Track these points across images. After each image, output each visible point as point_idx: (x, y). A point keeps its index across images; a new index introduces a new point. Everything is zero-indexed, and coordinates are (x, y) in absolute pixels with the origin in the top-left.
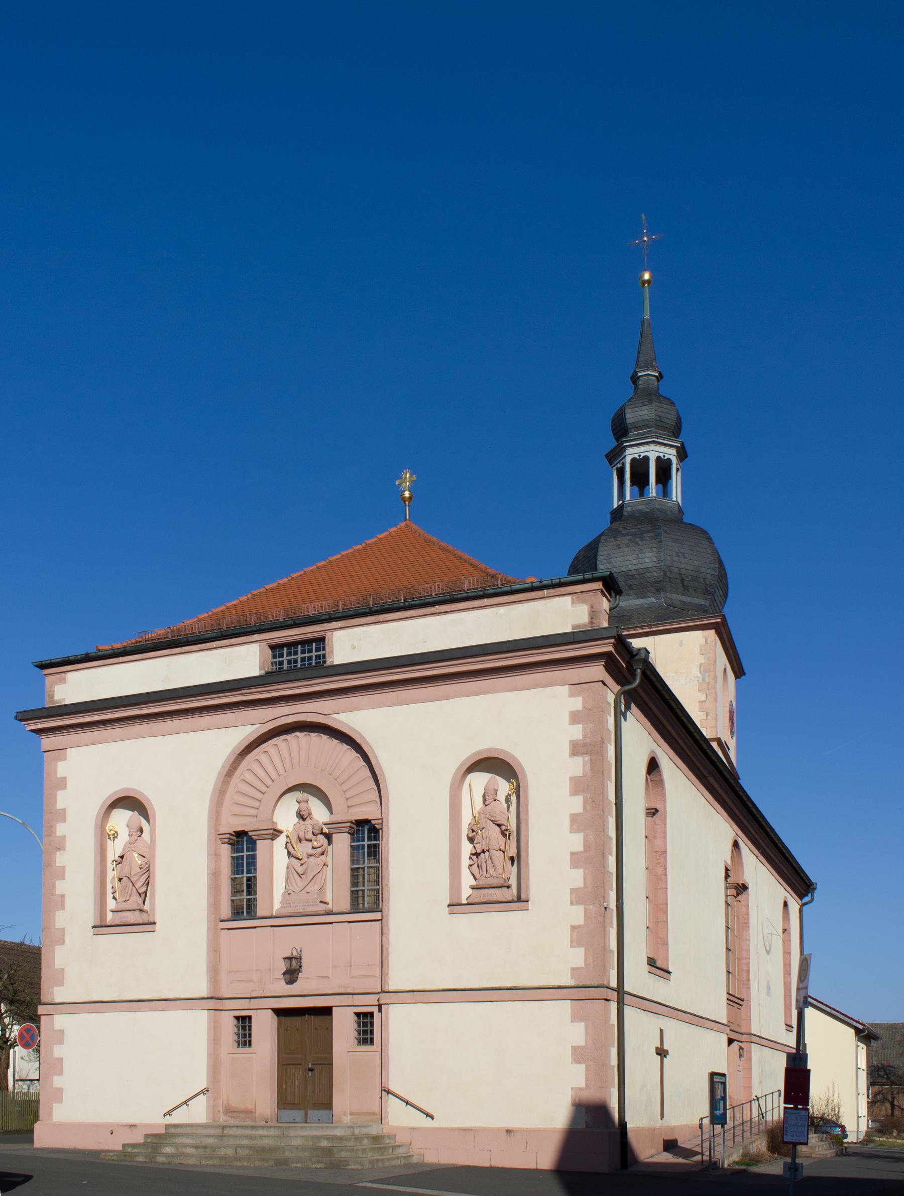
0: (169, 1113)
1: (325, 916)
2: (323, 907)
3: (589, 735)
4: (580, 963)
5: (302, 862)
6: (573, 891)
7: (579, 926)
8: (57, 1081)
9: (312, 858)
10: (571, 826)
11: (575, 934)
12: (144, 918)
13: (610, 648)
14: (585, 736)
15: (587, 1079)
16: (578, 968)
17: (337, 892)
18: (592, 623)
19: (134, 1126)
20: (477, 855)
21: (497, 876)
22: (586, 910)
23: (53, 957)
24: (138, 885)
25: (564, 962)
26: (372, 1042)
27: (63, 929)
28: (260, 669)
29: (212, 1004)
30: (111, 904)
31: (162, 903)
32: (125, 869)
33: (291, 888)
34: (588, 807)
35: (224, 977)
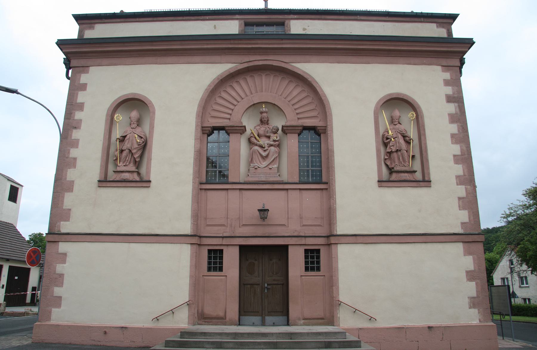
0: (157, 319)
4: (466, 220)
6: (457, 177)
7: (463, 198)
9: (272, 148)
10: (452, 140)
11: (461, 202)
14: (454, 94)
15: (477, 291)
16: (465, 223)
19: (126, 328)
20: (390, 153)
22: (466, 189)
23: (63, 202)
26: (318, 269)
27: (73, 181)
29: (195, 240)
30: (111, 168)
34: (461, 131)
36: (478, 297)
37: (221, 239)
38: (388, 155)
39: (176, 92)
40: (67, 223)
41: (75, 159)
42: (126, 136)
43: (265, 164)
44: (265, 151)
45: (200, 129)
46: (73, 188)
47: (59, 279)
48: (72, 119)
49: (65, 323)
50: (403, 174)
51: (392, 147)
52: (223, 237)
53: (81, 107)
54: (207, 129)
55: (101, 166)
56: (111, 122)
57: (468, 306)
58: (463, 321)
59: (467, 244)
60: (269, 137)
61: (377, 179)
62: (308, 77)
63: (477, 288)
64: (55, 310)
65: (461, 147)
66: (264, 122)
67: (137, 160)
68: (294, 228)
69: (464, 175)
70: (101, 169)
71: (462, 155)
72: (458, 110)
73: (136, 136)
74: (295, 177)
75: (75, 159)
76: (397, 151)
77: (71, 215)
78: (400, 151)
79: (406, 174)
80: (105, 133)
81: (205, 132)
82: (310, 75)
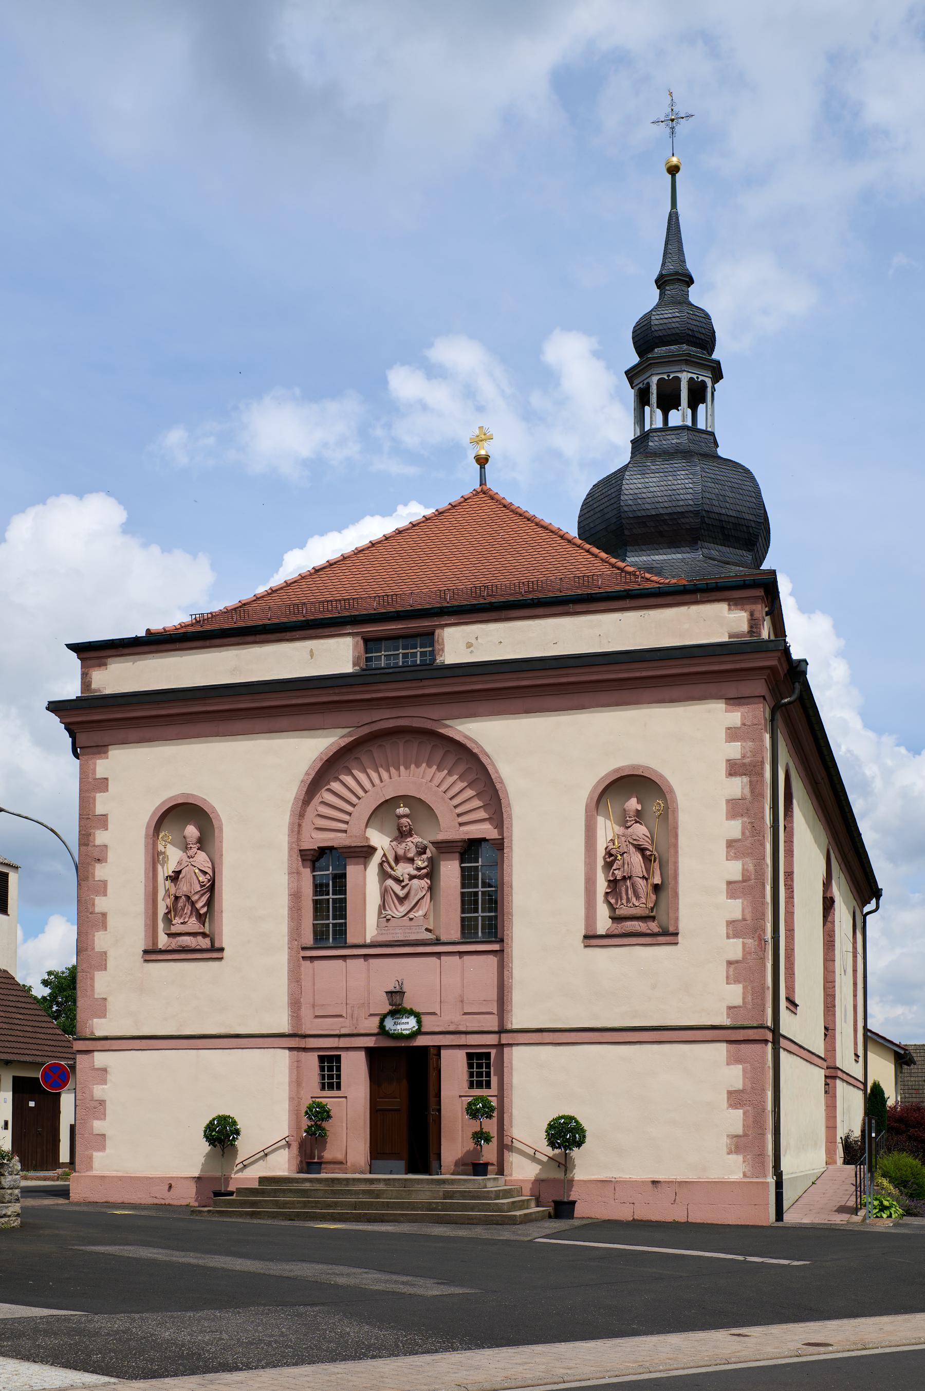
1: (427, 947)
2: (429, 936)
3: (749, 754)
4: (738, 1001)
5: (403, 884)
6: (729, 923)
7: (737, 962)
8: (98, 1126)
9: (415, 881)
10: (728, 852)
11: (731, 970)
12: (205, 943)
13: (774, 662)
14: (744, 757)
17: (450, 921)
18: (751, 632)
21: (637, 906)
22: (744, 944)
23: (93, 986)
24: (199, 905)
25: (719, 999)
27: (105, 953)
28: (354, 665)
29: (293, 1042)
31: (231, 926)
32: (184, 888)
33: (389, 912)
35: (306, 1013)
36: (745, 1135)
37: (337, 1039)
38: (611, 885)
39: (256, 783)
40: (103, 1020)
41: (104, 915)
42: (180, 872)
43: (403, 909)
44: (403, 887)
45: (296, 854)
46: (106, 964)
47: (99, 1108)
48: (91, 844)
49: (114, 1174)
50: (629, 923)
51: (616, 872)
52: (339, 1036)
53: (103, 784)
54: (308, 853)
55: (146, 925)
56: (155, 858)
57: (725, 1150)
58: (714, 1175)
59: (733, 1047)
60: (411, 860)
61: (583, 933)
62: (473, 745)
63: (744, 1120)
64: (97, 1155)
65: (743, 865)
66: (402, 834)
67: (202, 912)
68: (450, 1018)
69: (744, 919)
70: (146, 931)
71: (744, 881)
72: (747, 791)
73: (197, 871)
74: (452, 932)
75: (104, 915)
76: (624, 878)
77: (108, 1007)
78: (630, 878)
79: (635, 923)
80: (146, 869)
81: (305, 858)
82: (476, 743)
